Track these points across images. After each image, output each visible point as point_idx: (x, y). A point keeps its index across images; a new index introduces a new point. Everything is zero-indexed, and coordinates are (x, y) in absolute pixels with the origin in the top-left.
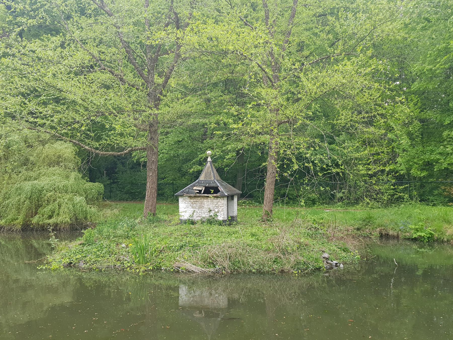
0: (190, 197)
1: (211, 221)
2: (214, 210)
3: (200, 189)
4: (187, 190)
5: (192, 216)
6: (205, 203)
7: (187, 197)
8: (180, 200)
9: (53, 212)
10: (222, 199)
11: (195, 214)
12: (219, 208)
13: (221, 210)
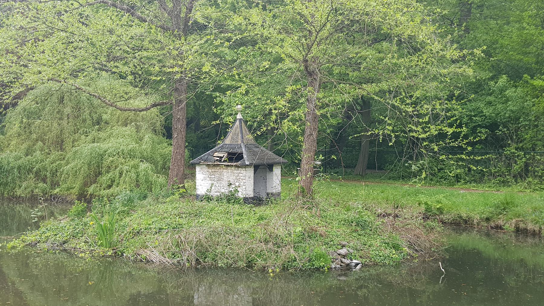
0: (208, 166)
1: (231, 198)
2: (234, 184)
3: (221, 155)
5: (209, 190)
7: (205, 166)
8: (198, 169)
9: (113, 181)
10: (244, 169)
11: (213, 188)
12: (244, 182)
13: (242, 184)
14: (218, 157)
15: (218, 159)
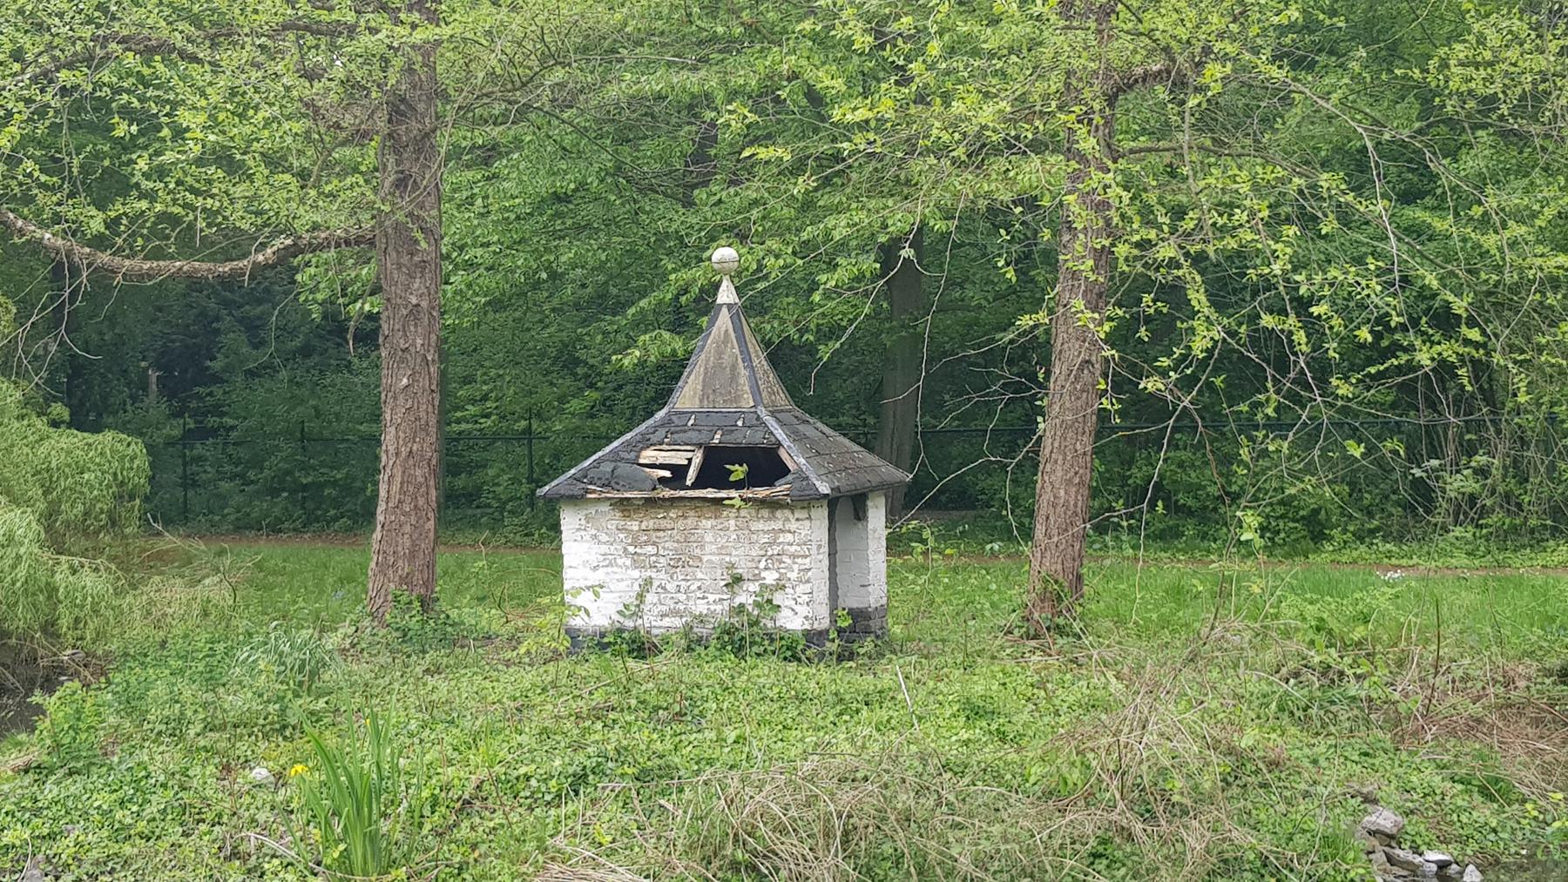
0: (624, 506)
1: (741, 639)
2: (757, 578)
3: (679, 459)
4: (607, 468)
6: (709, 538)
7: (605, 508)
8: (570, 520)
11: (650, 598)
12: (783, 564)
13: (793, 575)
14: (662, 467)
15: (667, 474)
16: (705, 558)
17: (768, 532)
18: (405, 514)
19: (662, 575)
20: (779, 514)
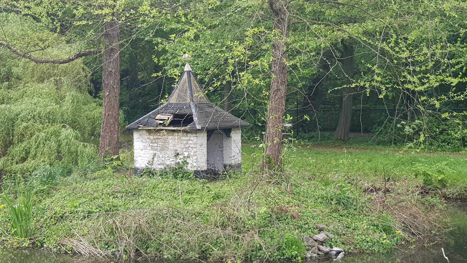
0: (149, 131)
1: (178, 172)
2: (183, 154)
4: (146, 120)
6: (170, 142)
7: (144, 132)
8: (136, 135)
9: (28, 153)
10: (194, 135)
11: (156, 159)
12: (194, 150)
13: (192, 154)
16: (169, 148)
17: (186, 140)
18: (107, 132)
19: (159, 152)
20: (188, 135)
